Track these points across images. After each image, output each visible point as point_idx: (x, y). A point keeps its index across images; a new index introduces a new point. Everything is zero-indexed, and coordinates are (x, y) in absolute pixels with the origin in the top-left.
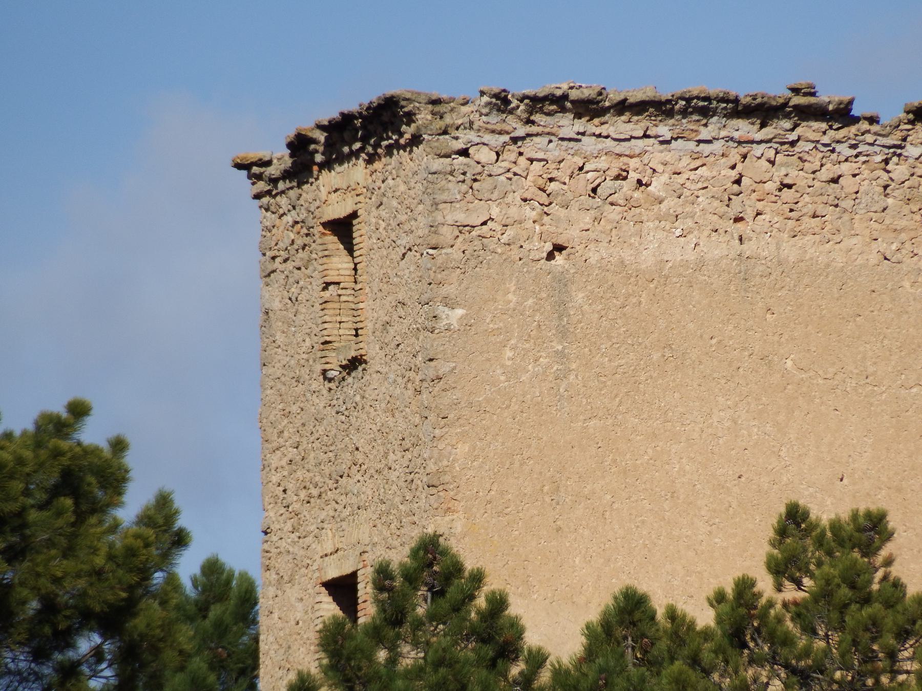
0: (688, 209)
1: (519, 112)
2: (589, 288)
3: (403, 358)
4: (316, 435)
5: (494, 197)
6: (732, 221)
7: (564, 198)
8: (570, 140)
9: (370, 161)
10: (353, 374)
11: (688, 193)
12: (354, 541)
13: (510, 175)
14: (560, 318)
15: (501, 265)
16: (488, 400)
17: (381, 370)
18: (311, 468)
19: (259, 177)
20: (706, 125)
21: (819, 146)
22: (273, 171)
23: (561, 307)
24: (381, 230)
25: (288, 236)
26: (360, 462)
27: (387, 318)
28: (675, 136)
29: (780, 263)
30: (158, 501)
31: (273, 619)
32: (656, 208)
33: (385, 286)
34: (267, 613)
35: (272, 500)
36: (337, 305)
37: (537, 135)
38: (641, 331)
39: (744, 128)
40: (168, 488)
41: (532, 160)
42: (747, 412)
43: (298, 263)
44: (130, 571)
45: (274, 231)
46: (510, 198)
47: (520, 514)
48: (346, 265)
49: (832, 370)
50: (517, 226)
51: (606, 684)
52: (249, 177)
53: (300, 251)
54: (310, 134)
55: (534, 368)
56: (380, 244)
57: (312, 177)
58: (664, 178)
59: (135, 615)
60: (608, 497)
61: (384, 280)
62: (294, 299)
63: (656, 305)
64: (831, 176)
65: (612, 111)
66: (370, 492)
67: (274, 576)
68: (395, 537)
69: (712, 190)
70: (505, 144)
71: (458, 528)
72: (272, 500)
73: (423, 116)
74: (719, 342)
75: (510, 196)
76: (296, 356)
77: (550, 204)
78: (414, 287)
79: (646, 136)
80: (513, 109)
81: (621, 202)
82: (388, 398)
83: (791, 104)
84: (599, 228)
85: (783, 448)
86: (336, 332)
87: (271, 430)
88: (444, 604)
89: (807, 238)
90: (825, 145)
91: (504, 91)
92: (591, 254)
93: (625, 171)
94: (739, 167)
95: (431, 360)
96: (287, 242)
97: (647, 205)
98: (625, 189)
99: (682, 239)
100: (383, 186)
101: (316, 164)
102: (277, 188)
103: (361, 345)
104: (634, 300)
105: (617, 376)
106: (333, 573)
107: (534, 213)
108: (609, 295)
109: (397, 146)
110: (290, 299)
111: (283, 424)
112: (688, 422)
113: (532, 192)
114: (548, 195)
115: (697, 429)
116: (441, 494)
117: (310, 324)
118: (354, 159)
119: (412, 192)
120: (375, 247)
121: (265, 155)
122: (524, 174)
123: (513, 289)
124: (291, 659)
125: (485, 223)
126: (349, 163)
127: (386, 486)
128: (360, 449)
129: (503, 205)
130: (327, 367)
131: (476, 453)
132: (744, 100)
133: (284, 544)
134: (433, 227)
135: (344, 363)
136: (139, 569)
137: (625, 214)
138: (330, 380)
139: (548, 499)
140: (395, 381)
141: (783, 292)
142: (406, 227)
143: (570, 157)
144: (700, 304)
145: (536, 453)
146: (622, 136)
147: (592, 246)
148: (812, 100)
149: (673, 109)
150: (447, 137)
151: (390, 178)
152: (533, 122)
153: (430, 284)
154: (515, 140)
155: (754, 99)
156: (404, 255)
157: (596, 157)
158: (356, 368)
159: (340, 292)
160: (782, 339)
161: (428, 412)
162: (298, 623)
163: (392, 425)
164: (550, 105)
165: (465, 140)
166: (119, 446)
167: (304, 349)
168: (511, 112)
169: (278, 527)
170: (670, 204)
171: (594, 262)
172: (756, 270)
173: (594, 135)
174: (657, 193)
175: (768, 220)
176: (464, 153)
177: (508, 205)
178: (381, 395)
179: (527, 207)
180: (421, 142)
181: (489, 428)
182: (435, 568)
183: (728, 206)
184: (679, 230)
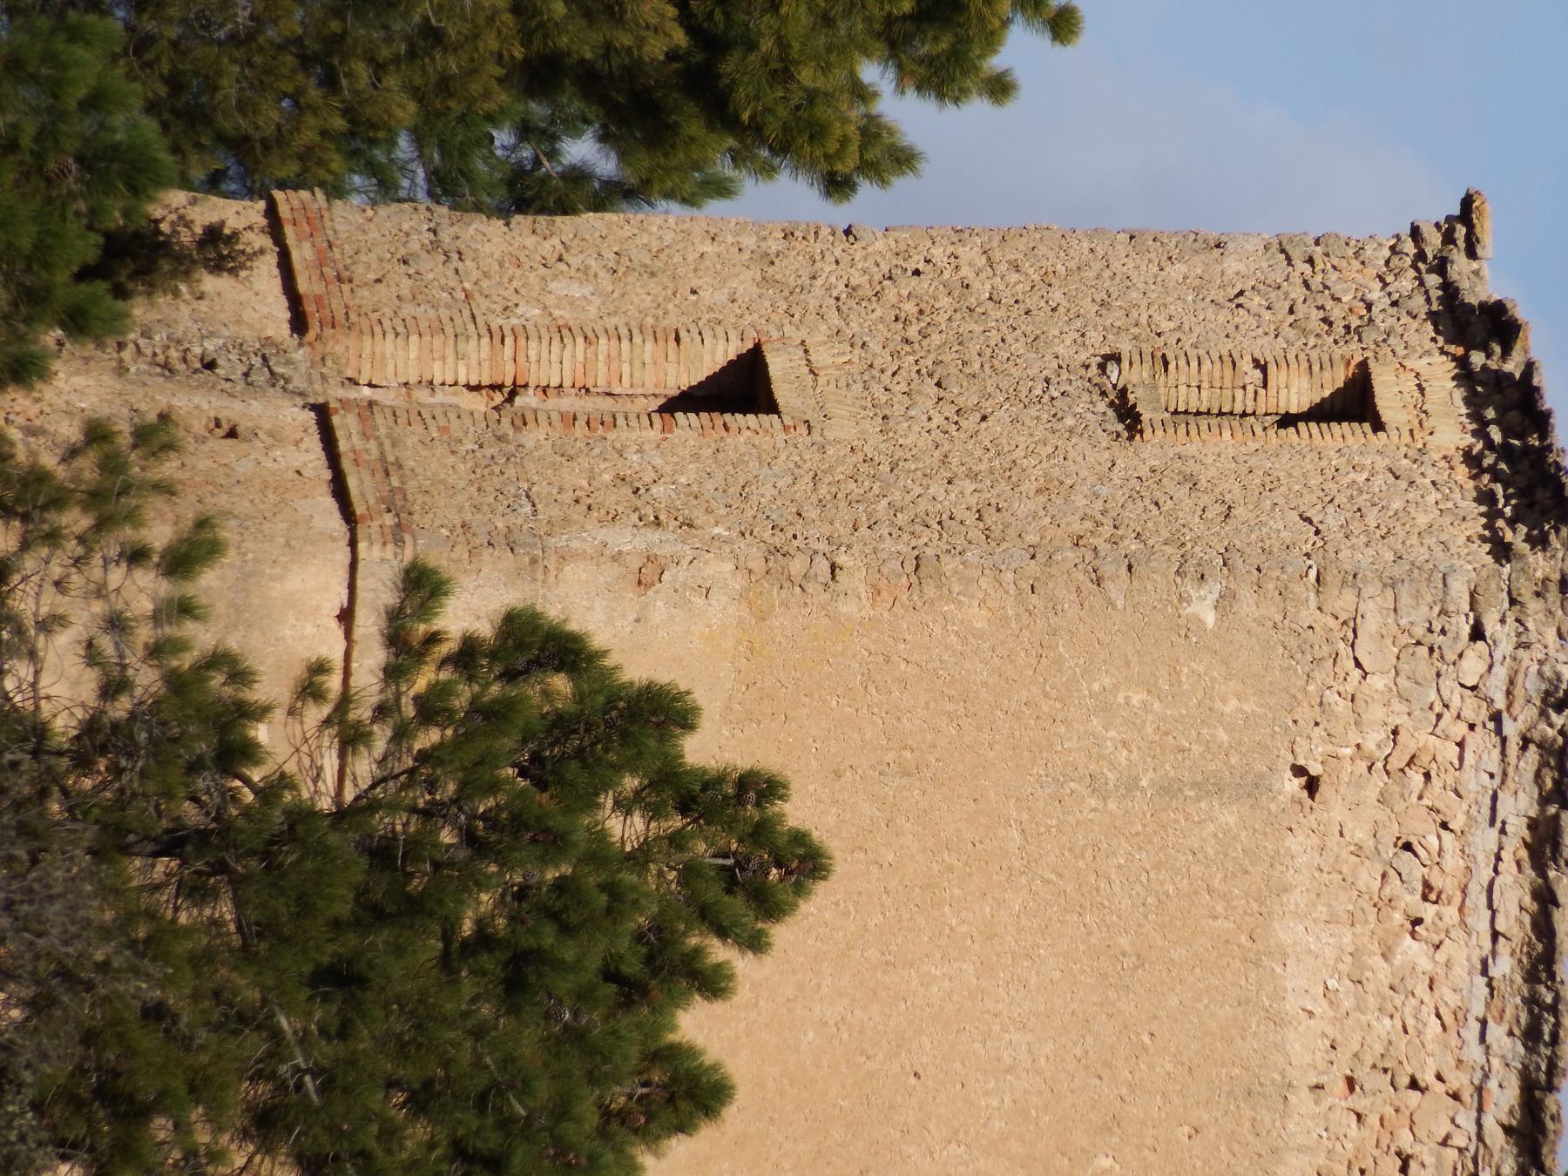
0: (1372, 1001)
1: (1543, 726)
2: (1244, 834)
3: (1133, 513)
4: (1009, 339)
5: (1402, 681)
6: (1349, 1073)
7: (1397, 796)
8: (1493, 809)
9: (1470, 459)
10: (1111, 413)
12: (831, 408)
14: (1195, 785)
15: (1286, 689)
16: (1059, 661)
17: (1116, 469)
18: (955, 325)
19: (1449, 238)
20: (1511, 1033)
22: (1460, 266)
23: (1210, 787)
24: (1353, 475)
25: (1346, 291)
28: (1495, 984)
30: (902, 149)
31: (702, 242)
32: (1375, 948)
33: (1258, 481)
34: (713, 231)
35: (902, 247)
36: (1227, 383)
37: (1503, 753)
38: (1167, 919)
39: (1505, 1098)
40: (922, 166)
41: (1461, 744)
42: (1026, 1091)
43: (1301, 310)
44: (786, 129)
45: (1356, 264)
46: (1398, 706)
48: (1294, 400)
51: (569, 1165)
52: (1449, 219)
53: (1321, 314)
54: (1518, 346)
56: (1329, 473)
57: (1447, 341)
58: (1425, 964)
59: (710, 126)
60: (890, 858)
61: (1268, 479)
62: (1241, 300)
65: (1540, 881)
67: (774, 248)
68: (834, 490)
69: (1401, 1042)
70: (1490, 702)
71: (847, 608)
74: (1145, 1048)
75: (1404, 708)
76: (1144, 304)
77: (1388, 773)
78: (1253, 536)
79: (1495, 935)
80: (1548, 718)
81: (1387, 891)
82: (1069, 482)
84: (1344, 854)
86: (1183, 379)
87: (1022, 247)
88: (713, 892)
92: (1301, 838)
93: (1438, 897)
94: (1439, 1088)
95: (1130, 567)
96: (1337, 289)
98: (1408, 898)
99: (1321, 991)
100: (1427, 481)
101: (1467, 350)
102: (1429, 271)
103: (1159, 432)
104: (1219, 908)
106: (778, 365)
107: (1373, 747)
108: (1230, 866)
109: (1493, 515)
110: (1241, 293)
111: (1031, 271)
112: (1012, 993)
113: (1408, 743)
114: (1402, 770)
115: (1000, 1006)
116: (904, 579)
117: (1197, 330)
118: (1474, 426)
119: (1414, 540)
120: (1324, 463)
121: (1486, 248)
122: (1438, 731)
123: (1246, 708)
124: (631, 278)
125: (1358, 664)
126: (1468, 416)
127: (919, 474)
128: (984, 425)
129: (1387, 697)
130: (1125, 364)
131: (971, 640)
132: (1551, 1102)
133: (827, 269)
134: (1353, 578)
135: (1131, 397)
137: (1366, 897)
139: (890, 757)
141: (1225, 1154)
142: (1356, 526)
143: (1465, 807)
145: (967, 739)
147: (1315, 840)
149: (1539, 981)
150: (1506, 605)
151: (1439, 496)
152: (1524, 748)
153: (1259, 570)
154: (1496, 717)
155: (1552, 1118)
156: (1309, 520)
157: (1462, 851)
158: (1121, 419)
159: (1250, 389)
160: (1146, 1152)
161: (1043, 560)
162: (694, 292)
164: (1554, 779)
165: (1498, 636)
166: (1000, 88)
167: (1156, 317)
168: (1543, 713)
170: (1380, 972)
172: (1264, 1112)
173: (1501, 848)
175: (1349, 1133)
176: (1477, 634)
177: (1387, 704)
178: (1073, 468)
179: (1383, 735)
180: (1497, 560)
181: (1012, 662)
182: (774, 871)
183: (1374, 1066)
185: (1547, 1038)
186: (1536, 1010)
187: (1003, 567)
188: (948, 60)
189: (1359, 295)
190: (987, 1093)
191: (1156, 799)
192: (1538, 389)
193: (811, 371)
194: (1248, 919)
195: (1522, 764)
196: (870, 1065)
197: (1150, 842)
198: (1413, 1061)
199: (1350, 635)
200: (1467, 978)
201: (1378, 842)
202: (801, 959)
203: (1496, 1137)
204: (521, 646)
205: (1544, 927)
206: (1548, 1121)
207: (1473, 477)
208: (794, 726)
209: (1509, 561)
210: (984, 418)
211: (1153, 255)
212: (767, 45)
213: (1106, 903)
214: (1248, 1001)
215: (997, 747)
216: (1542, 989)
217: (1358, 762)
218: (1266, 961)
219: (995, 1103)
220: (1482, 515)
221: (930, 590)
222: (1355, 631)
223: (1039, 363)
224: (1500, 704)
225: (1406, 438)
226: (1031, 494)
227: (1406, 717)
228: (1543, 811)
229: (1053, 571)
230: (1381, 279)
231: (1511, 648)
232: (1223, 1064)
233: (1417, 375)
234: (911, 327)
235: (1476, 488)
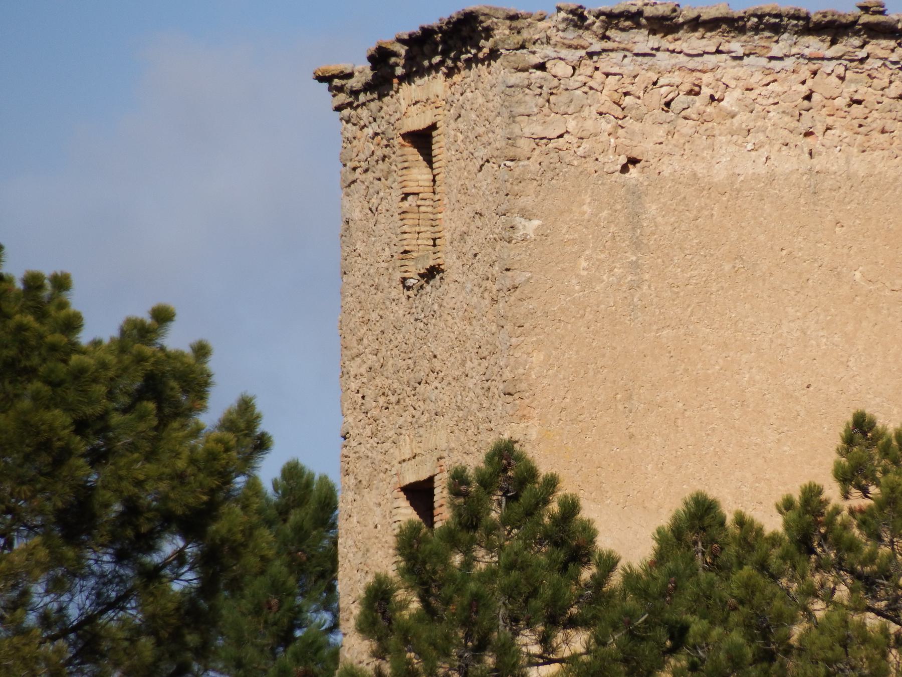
1: (595, 28)
2: (662, 200)
4: (395, 343)
5: (570, 111)
7: (638, 112)
8: (644, 55)
9: (449, 75)
10: (431, 283)
14: (634, 229)
15: (577, 178)
18: (390, 375)
19: (340, 89)
20: (777, 42)
21: (888, 63)
22: (354, 83)
23: (635, 219)
24: (459, 142)
25: (369, 148)
27: (464, 229)
28: (747, 52)
30: (239, 406)
32: (728, 122)
36: (416, 216)
37: (612, 50)
39: (814, 45)
40: (250, 393)
41: (607, 75)
42: (817, 322)
43: (378, 175)
44: (211, 474)
45: (355, 142)
50: (593, 139)
51: (675, 588)
52: (330, 89)
53: (380, 162)
54: (391, 47)
55: (608, 277)
56: (459, 156)
57: (392, 89)
60: (680, 405)
61: (462, 191)
62: (374, 209)
63: (728, 218)
65: (685, 27)
66: (447, 399)
68: (472, 443)
71: (534, 434)
73: (501, 31)
74: (789, 254)
75: (587, 109)
76: (377, 265)
77: (625, 117)
78: (490, 199)
79: (718, 52)
81: (694, 116)
82: (465, 306)
83: (860, 22)
84: (673, 142)
86: (414, 242)
89: (876, 153)
91: (581, 7)
92: (664, 167)
93: (697, 85)
94: (810, 83)
95: (508, 270)
96: (368, 153)
98: (698, 104)
99: (753, 153)
100: (461, 98)
102: (357, 100)
103: (439, 255)
106: (410, 478)
107: (609, 126)
109: (475, 60)
110: (370, 209)
111: (363, 331)
112: (759, 332)
113: (608, 106)
114: (623, 109)
115: (767, 339)
116: (517, 402)
117: (389, 234)
119: (490, 105)
120: (454, 158)
122: (600, 88)
123: (588, 200)
124: (369, 562)
125: (561, 136)
126: (429, 75)
128: (438, 356)
130: (406, 275)
132: (815, 18)
133: (363, 449)
135: (422, 271)
136: (220, 473)
138: (409, 288)
139: (620, 407)
141: (853, 205)
142: (484, 139)
143: (644, 72)
144: (771, 216)
147: (665, 159)
149: (744, 25)
150: (525, 51)
151: (468, 90)
152: (609, 38)
153: (507, 195)
154: (591, 55)
155: (825, 16)
157: (670, 72)
158: (434, 277)
159: (419, 202)
162: (376, 527)
164: (625, 21)
166: (202, 351)
167: (383, 258)
168: (587, 28)
170: (743, 118)
171: (667, 175)
172: (826, 184)
173: (668, 50)
174: (729, 109)
176: (542, 67)
177: (585, 119)
178: (458, 304)
179: (603, 120)
183: (798, 121)
184: (750, 144)
185: (777, 20)
186: (762, 26)
187: (508, 344)
188: (185, 381)
189: (371, 140)
190: (818, 345)
191: (643, 251)
192: (410, 35)
193: (414, 457)
194: (713, 195)
195: (617, 39)
196: (802, 414)
197: (668, 254)
198: (795, 98)
200: (745, 68)
201: (665, 122)
202: (741, 455)
204: (374, 623)
205: (713, 24)
206: (826, 20)
207: (459, 71)
208: (604, 463)
209: (498, 50)
210: (435, 357)
211: (353, 260)
212: (163, 486)
213: (704, 279)
214: (761, 195)
215: (614, 345)
216: (749, 24)
217: (618, 135)
218: (737, 186)
219: (824, 340)
220: (477, 66)
221: (523, 386)
223: (408, 325)
224: (582, 53)
225: (440, 111)
226: (472, 328)
229: (510, 315)
231: (549, 47)
234: (391, 400)
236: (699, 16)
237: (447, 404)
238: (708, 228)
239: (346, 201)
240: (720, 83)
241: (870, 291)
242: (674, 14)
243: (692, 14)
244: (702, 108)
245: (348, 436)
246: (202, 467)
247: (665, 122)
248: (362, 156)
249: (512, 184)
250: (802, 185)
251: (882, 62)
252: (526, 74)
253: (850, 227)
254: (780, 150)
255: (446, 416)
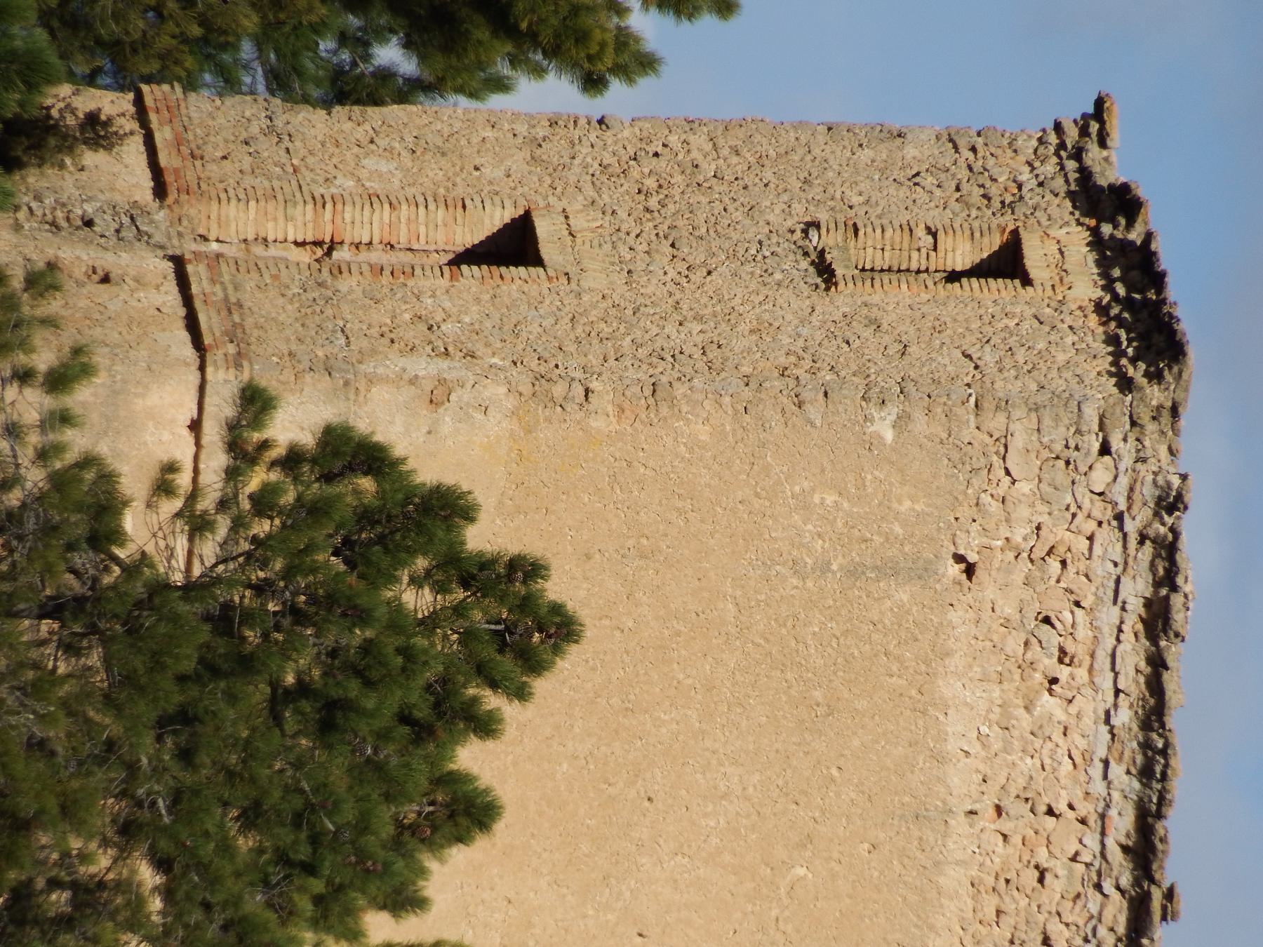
0: (1017, 744)
1: (1157, 525)
2: (915, 609)
4: (731, 208)
5: (1043, 486)
8: (1116, 592)
9: (1101, 309)
10: (812, 269)
11: (1037, 746)
12: (586, 263)
13: (1073, 509)
15: (950, 493)
18: (686, 197)
19: (1084, 132)
20: (1128, 772)
21: (1094, 922)
22: (1094, 153)
23: (888, 570)
24: (1006, 321)
25: (1001, 174)
26: (692, 276)
27: (885, 326)
29: (937, 864)
32: (1020, 702)
36: (906, 245)
37: (1125, 547)
38: (853, 676)
39: (1123, 823)
40: (664, 69)
41: (1091, 538)
42: (738, 813)
43: (965, 187)
44: (557, 36)
45: (1009, 153)
46: (1041, 508)
47: (611, 506)
49: (789, 928)
50: (1003, 516)
51: (367, 871)
52: (1084, 116)
53: (982, 191)
54: (1140, 220)
55: (809, 531)
56: (987, 319)
60: (630, 624)
61: (937, 323)
62: (917, 180)
63: (886, 696)
64: (1053, 937)
65: (1153, 649)
66: (649, 290)
68: (588, 329)
69: (1040, 777)
71: (597, 423)
72: (645, 134)
73: (1155, 395)
74: (833, 780)
75: (1045, 509)
76: (838, 182)
77: (1032, 561)
78: (925, 370)
79: (1117, 692)
80: (1162, 518)
81: (1029, 655)
82: (776, 324)
83: (1154, 889)
84: (995, 626)
85: (687, 859)
86: (870, 243)
87: (741, 136)
88: (488, 652)
89: (969, 901)
90: (1094, 930)
91: (1186, 508)
92: (960, 613)
93: (1071, 661)
94: (1071, 815)
95: (826, 394)
96: (995, 172)
97: (1024, 689)
98: (1047, 661)
100: (1066, 326)
102: (1069, 158)
103: (851, 285)
104: (894, 668)
105: (793, 643)
106: (543, 228)
107: (1019, 540)
109: (1118, 354)
110: (918, 174)
113: (1048, 538)
114: (1043, 559)
115: (717, 745)
116: (643, 401)
117: (883, 203)
119: (1054, 373)
120: (982, 311)
121: (1115, 139)
122: (1073, 527)
123: (917, 507)
124: (428, 156)
125: (1008, 473)
126: (1099, 274)
128: (709, 278)
130: (824, 231)
131: (696, 449)
132: (1160, 827)
133: (584, 151)
134: (1004, 405)
135: (828, 257)
136: (558, 47)
138: (805, 232)
139: (630, 543)
140: (799, 336)
142: (1008, 362)
144: (886, 755)
146: (1118, 660)
147: (971, 615)
148: (1157, 915)
150: (1128, 427)
151: (1076, 338)
152: (1141, 543)
153: (929, 396)
154: (1119, 517)
155: (1161, 840)
156: (969, 357)
158: (820, 274)
159: (924, 251)
160: (833, 864)
162: (477, 169)
163: (740, 329)
164: (1165, 568)
165: (1121, 452)
167: (848, 192)
168: (1156, 514)
169: (609, 142)
170: (1024, 721)
171: (949, 617)
172: (929, 832)
173: (1122, 622)
174: (1039, 703)
175: (997, 849)
176: (1105, 450)
177: (1032, 505)
178: (781, 313)
180: (1122, 391)
181: (729, 468)
183: (1018, 796)
184: (987, 731)
190: (706, 815)
192: (1155, 254)
195: (1140, 554)
199: (1002, 450)
201: (1023, 616)
202: (558, 705)
203: (1115, 854)
204: (336, 454)
205: (1155, 686)
207: (1103, 324)
208: (553, 517)
209: (1131, 392)
210: (709, 273)
211: (846, 143)
216: (1154, 736)
218: (931, 711)
219: (712, 824)
220: (1109, 354)
222: (1006, 447)
225: (1049, 292)
226: (746, 333)
227: (1046, 516)
228: (1156, 592)
229: (763, 396)
230: (1029, 164)
232: (896, 793)
233: (1058, 242)
235: (1105, 332)
236: (1167, 668)
237: (642, 291)
238: (874, 669)
239: (927, 135)
240: (1075, 693)
241: (778, 888)
242: (1172, 635)
243: (1170, 661)
244: (1041, 667)
245: (604, 127)
246: (568, 22)
247: (1023, 616)
248: (991, 162)
249: (945, 404)
250: (929, 800)
251: (1095, 914)
252: (1096, 428)
253: (868, 863)
254: (978, 771)
255: (626, 288)
